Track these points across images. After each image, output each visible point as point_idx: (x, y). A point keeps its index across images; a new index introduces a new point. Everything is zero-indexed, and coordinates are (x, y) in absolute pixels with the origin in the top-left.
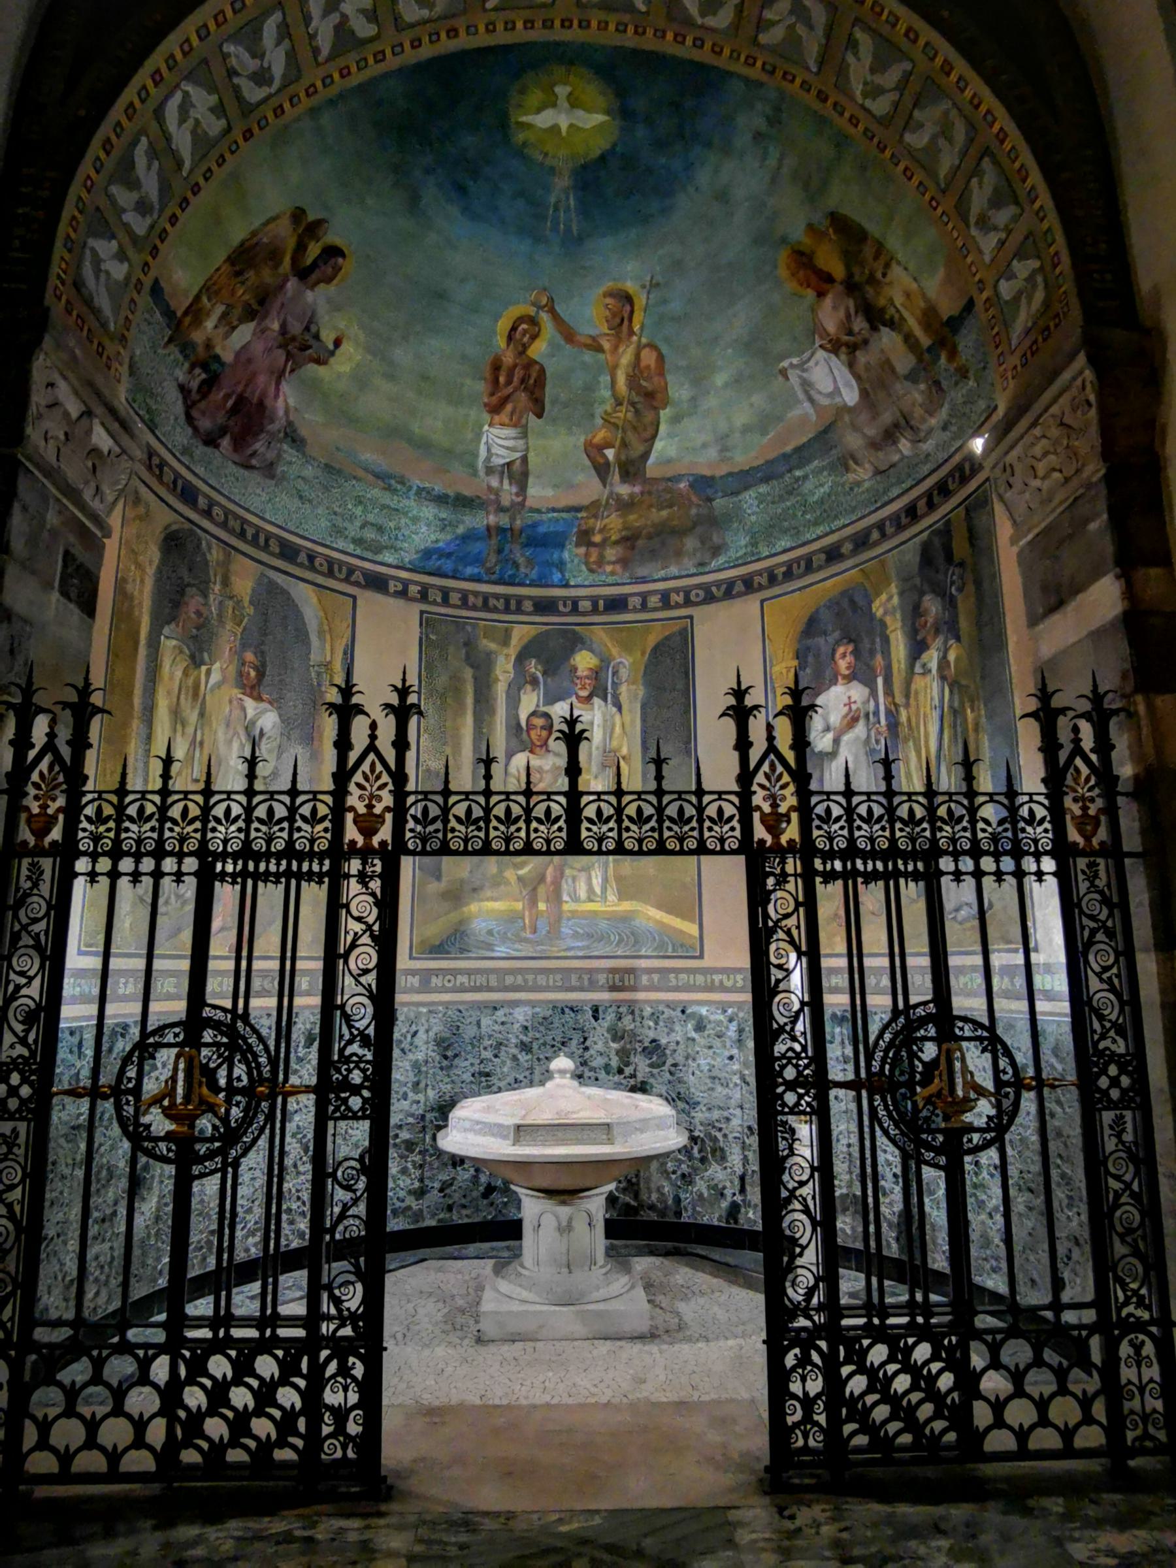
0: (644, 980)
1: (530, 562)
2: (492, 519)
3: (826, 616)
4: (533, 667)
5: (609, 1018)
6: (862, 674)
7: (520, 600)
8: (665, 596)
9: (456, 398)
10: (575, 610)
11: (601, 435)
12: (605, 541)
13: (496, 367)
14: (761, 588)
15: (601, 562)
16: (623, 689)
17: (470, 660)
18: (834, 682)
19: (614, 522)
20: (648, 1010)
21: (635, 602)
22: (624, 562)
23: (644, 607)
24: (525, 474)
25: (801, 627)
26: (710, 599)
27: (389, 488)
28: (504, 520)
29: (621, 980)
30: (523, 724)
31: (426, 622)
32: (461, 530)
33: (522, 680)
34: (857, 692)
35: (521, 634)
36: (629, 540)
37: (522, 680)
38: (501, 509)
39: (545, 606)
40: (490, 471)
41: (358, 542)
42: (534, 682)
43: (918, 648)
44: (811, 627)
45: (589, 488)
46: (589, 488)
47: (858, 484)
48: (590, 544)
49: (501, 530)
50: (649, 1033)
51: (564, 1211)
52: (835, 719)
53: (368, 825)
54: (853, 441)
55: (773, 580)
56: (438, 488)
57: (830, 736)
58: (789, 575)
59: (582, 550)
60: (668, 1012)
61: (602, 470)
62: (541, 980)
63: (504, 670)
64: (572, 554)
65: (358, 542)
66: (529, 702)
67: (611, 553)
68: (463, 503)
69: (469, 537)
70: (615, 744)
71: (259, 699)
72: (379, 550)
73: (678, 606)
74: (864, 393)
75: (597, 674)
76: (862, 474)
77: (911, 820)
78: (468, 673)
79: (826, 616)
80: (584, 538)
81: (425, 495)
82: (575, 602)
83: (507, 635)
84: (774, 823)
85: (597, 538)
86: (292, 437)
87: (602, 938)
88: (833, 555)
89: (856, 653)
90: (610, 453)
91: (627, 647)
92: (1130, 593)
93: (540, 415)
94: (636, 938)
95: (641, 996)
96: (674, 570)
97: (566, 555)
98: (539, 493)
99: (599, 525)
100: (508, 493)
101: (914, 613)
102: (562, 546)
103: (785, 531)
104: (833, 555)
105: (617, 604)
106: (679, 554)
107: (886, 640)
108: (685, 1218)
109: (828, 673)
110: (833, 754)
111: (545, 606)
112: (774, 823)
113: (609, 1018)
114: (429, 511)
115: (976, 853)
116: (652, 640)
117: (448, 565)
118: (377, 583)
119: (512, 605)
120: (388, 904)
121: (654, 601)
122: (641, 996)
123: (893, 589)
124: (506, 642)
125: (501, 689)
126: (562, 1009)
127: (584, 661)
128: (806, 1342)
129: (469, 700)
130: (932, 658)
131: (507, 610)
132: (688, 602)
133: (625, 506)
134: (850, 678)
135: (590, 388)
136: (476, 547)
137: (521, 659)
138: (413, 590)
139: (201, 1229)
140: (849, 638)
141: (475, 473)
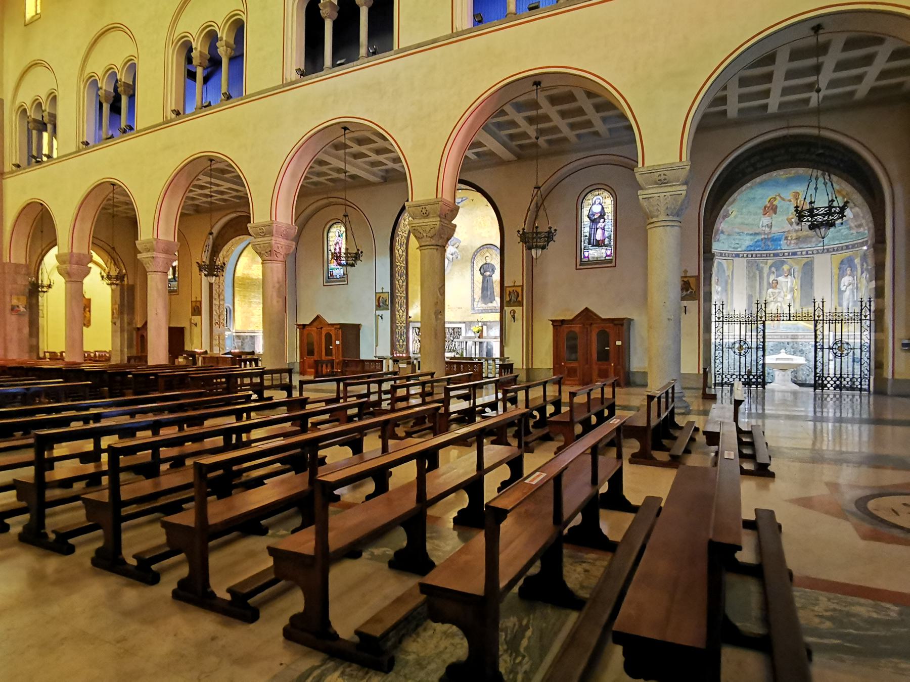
0: (800, 337)
1: (772, 245)
2: (763, 237)
3: (845, 261)
4: (773, 269)
5: (791, 345)
6: (852, 275)
7: (770, 254)
8: (807, 252)
9: (756, 214)
10: (784, 255)
11: (790, 217)
12: (791, 239)
13: (765, 207)
14: (831, 252)
15: (790, 243)
16: (796, 273)
17: (758, 269)
18: (846, 275)
19: (794, 235)
20: (800, 343)
21: (799, 253)
22: (797, 244)
23: (802, 254)
24: (771, 226)
25: (840, 262)
26: (818, 253)
27: (740, 235)
28: (766, 237)
29: (794, 337)
30: (771, 282)
31: (748, 262)
32: (756, 240)
33: (771, 272)
34: (851, 278)
35: (770, 262)
36: (798, 238)
37: (771, 272)
38: (765, 234)
39: (775, 255)
40: (762, 227)
41: (734, 248)
42: (774, 273)
43: (862, 273)
44: (842, 262)
45: (787, 227)
46: (787, 227)
47: (852, 233)
48: (787, 240)
49: (765, 238)
50: (801, 347)
51: (783, 373)
52: (846, 284)
53: (761, 318)
54: (853, 225)
55: (834, 250)
56: (751, 233)
57: (845, 287)
58: (837, 250)
59: (786, 241)
60: (805, 344)
61: (791, 224)
62: (775, 337)
63: (766, 270)
64: (783, 242)
65: (734, 248)
66: (772, 278)
67: (793, 242)
68: (756, 234)
69: (758, 241)
70: (793, 286)
71: (717, 285)
72: (737, 248)
73: (810, 254)
74: (854, 216)
75: (789, 270)
76: (854, 232)
77: (839, 316)
78: (757, 272)
79: (845, 261)
80: (786, 238)
81: (747, 234)
82: (784, 253)
83: (767, 262)
84: (819, 317)
85: (789, 238)
86: (722, 232)
87: (790, 328)
88: (847, 247)
89: (851, 270)
90: (793, 220)
91: (797, 264)
92: (876, 285)
93: (775, 213)
94: (798, 328)
95: (799, 340)
96: (809, 246)
97: (781, 242)
98: (774, 229)
99: (790, 235)
100: (767, 230)
101: (862, 265)
102: (780, 241)
103: (838, 240)
104: (847, 247)
105: (794, 254)
106: (811, 242)
107: (857, 268)
108: (807, 382)
109: (845, 274)
110: (845, 291)
111: (775, 255)
112: (819, 317)
113: (791, 345)
114: (749, 237)
115: (848, 320)
116: (803, 262)
117: (752, 248)
118: (737, 256)
119: (767, 255)
120: (764, 326)
121: (804, 253)
122: (799, 340)
123: (859, 258)
124: (766, 263)
125: (765, 275)
126: (780, 343)
127: (786, 267)
128: (819, 377)
129: (758, 278)
130: (864, 275)
131: (767, 256)
132: (813, 253)
133: (796, 231)
134: (850, 275)
135: (788, 208)
136: (758, 243)
137: (770, 267)
138: (745, 255)
139: (743, 365)
140: (850, 266)
141: (759, 227)
